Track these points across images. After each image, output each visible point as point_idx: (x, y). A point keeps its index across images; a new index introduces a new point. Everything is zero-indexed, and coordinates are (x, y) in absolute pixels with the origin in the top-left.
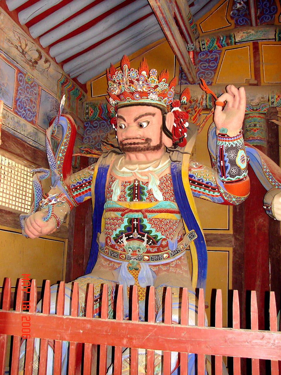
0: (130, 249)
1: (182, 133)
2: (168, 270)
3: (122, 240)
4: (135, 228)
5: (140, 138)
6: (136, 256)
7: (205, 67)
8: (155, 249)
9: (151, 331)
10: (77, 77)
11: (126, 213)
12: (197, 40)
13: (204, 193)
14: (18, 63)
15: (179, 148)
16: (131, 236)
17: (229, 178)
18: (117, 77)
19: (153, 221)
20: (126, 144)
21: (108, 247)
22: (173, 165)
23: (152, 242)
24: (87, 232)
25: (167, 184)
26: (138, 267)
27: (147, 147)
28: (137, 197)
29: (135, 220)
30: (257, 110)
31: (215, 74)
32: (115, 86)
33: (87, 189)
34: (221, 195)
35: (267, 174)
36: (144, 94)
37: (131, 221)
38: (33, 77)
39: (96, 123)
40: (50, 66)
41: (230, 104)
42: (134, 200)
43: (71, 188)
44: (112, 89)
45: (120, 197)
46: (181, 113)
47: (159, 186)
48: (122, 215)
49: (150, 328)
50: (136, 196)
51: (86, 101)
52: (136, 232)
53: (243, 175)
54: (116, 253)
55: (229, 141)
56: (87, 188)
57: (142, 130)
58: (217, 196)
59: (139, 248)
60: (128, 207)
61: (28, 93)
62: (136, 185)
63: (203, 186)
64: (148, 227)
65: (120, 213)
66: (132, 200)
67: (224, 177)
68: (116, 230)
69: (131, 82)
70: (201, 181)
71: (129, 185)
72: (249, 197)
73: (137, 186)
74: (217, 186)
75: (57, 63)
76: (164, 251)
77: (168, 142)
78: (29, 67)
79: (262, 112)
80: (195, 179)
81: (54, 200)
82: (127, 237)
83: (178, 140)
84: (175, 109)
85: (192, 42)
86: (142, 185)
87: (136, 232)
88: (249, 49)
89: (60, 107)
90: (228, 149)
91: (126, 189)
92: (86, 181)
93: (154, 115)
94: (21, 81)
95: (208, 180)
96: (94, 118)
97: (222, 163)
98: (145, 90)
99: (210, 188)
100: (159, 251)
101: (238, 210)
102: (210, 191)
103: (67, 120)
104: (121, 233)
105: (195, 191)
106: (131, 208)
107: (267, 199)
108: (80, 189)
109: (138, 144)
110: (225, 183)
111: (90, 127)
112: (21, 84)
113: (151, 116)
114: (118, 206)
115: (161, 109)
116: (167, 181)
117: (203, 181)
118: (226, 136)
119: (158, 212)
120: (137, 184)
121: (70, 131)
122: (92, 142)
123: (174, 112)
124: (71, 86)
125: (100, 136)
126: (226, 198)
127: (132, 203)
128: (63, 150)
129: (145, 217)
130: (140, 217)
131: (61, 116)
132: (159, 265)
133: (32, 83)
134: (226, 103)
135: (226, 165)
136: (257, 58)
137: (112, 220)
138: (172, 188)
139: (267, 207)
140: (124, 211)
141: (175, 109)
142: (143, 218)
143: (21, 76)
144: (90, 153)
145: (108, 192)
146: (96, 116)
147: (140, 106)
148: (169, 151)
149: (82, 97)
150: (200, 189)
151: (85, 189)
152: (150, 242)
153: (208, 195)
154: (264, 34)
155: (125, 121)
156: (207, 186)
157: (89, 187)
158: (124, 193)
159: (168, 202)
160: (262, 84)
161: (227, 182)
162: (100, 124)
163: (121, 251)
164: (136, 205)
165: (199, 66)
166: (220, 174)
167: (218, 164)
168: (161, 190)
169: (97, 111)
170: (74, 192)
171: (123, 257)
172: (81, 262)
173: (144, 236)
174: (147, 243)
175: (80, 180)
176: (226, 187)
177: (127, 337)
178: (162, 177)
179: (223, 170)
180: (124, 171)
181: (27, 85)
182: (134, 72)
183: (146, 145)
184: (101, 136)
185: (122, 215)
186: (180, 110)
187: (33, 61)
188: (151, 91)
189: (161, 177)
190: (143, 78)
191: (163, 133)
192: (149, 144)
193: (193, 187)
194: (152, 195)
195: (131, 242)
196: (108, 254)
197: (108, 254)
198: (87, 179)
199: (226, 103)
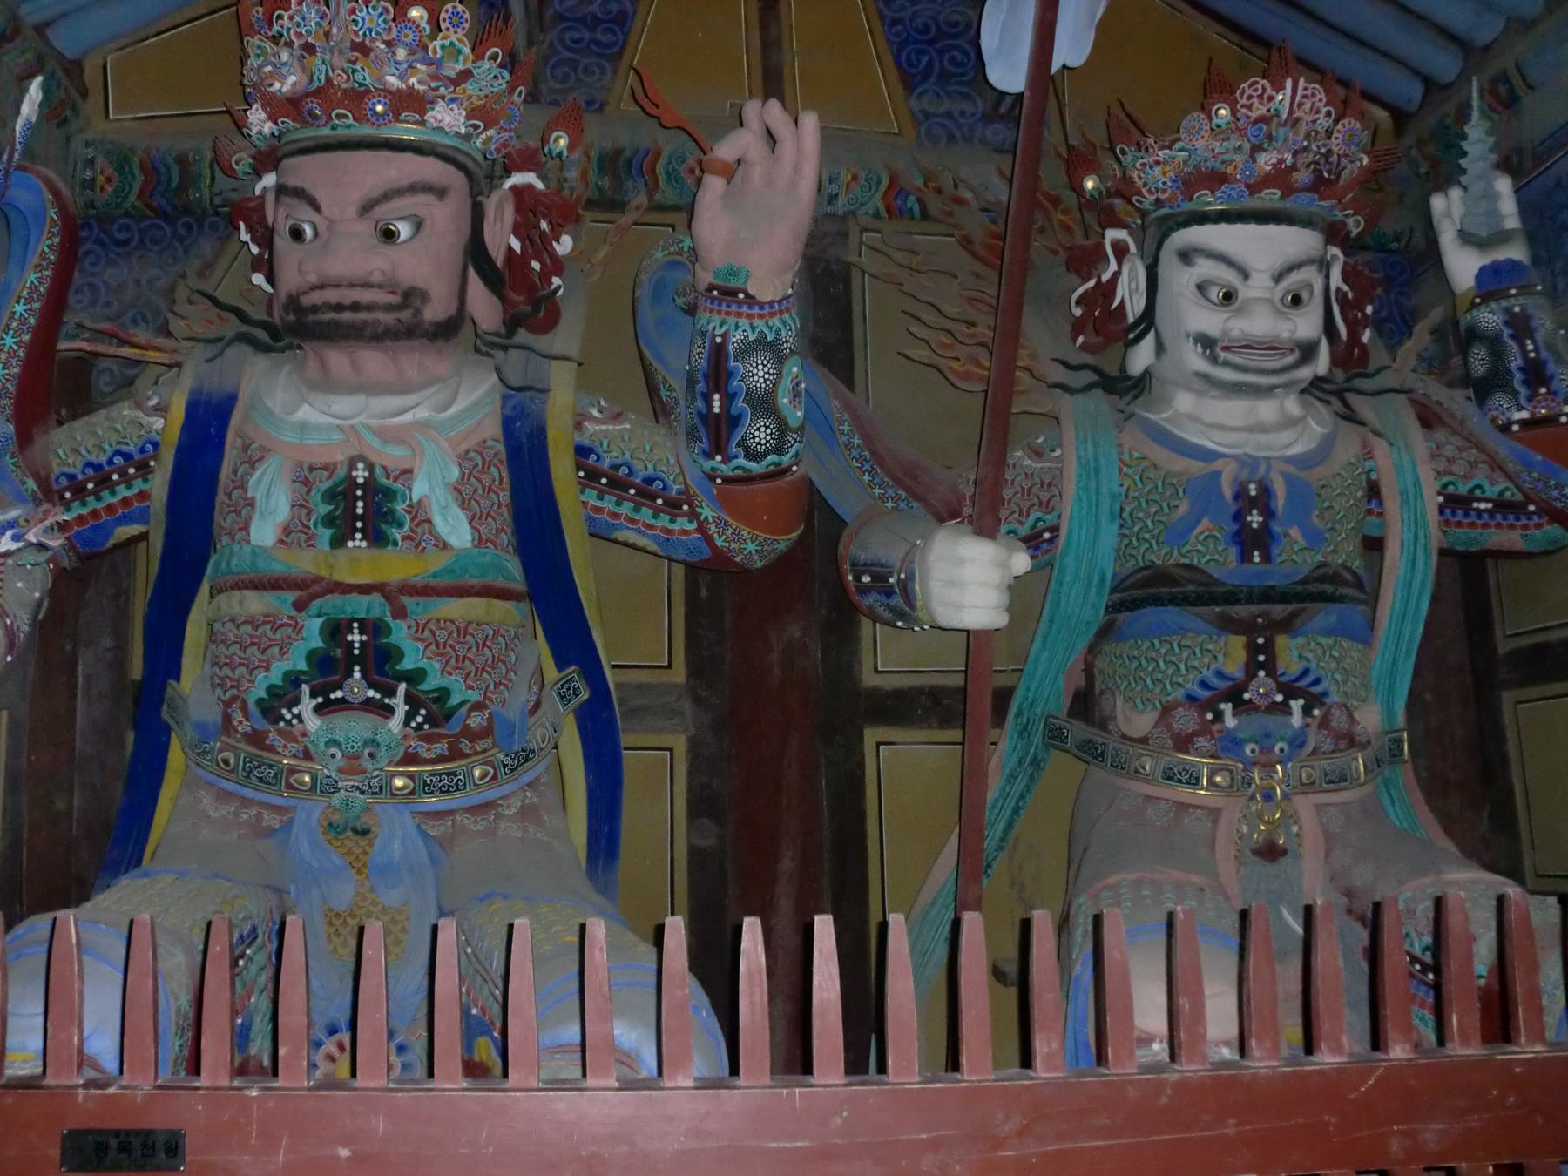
0: (333, 750)
1: (545, 276)
2: (491, 832)
3: (295, 711)
4: (356, 661)
5: (380, 286)
6: (360, 777)
7: (577, 41)
8: (441, 748)
13: (633, 521)
15: (523, 336)
16: (339, 694)
17: (742, 461)
18: (297, 19)
19: (433, 633)
20: (315, 309)
21: (231, 741)
22: (510, 404)
23: (427, 719)
24: (88, 678)
25: (486, 479)
26: (365, 821)
28: (361, 531)
29: (355, 625)
31: (615, 72)
32: (285, 56)
33: (128, 493)
34: (702, 529)
35: (854, 453)
36: (409, 103)
37: (335, 630)
39: (127, 228)
42: (350, 544)
43: (56, 487)
44: (269, 68)
45: (287, 530)
47: (456, 489)
48: (300, 606)
50: (359, 524)
51: (81, 130)
52: (357, 675)
53: (792, 451)
54: (271, 767)
55: (750, 317)
56: (129, 487)
57: (390, 250)
58: (686, 532)
59: (373, 742)
60: (324, 573)
63: (632, 491)
65: (291, 596)
66: (338, 542)
67: (719, 458)
68: (267, 669)
69: (363, 49)
70: (623, 471)
71: (330, 477)
72: (801, 537)
73: (363, 486)
74: (686, 491)
76: (477, 753)
77: (484, 307)
80: (598, 465)
81: (9, 533)
82: (320, 700)
83: (526, 299)
84: (518, 179)
86: (384, 481)
87: (357, 675)
91: (316, 497)
92: (127, 457)
93: (441, 192)
95: (650, 467)
96: (118, 206)
97: (716, 404)
99: (660, 501)
100: (455, 754)
101: (704, 593)
103: (45, 190)
104: (294, 680)
105: (598, 510)
106: (337, 577)
108: (96, 494)
109: (370, 308)
110: (719, 481)
111: (99, 242)
113: (429, 198)
114: (278, 568)
116: (486, 466)
117: (631, 473)
118: (741, 296)
119: (451, 595)
120: (360, 474)
121: (57, 240)
122: (108, 304)
124: (29, 56)
125: (144, 282)
126: (719, 543)
127: (340, 553)
129: (400, 613)
130: (376, 613)
131: (19, 168)
132: (451, 812)
135: (734, 412)
137: (248, 628)
138: (505, 496)
140: (307, 590)
141: (518, 179)
142: (389, 619)
144: (123, 342)
145: (226, 509)
146: (126, 197)
147: (385, 154)
148: (484, 349)
149: (68, 113)
150: (618, 504)
151: (122, 492)
152: (419, 719)
153: (651, 527)
155: (317, 208)
156: (646, 493)
157: (138, 485)
158: (304, 511)
159: (490, 554)
161: (726, 480)
162: (140, 230)
163: (294, 756)
164: (358, 560)
165: (552, 36)
166: (705, 444)
167: (700, 404)
168: (464, 504)
169: (134, 177)
172: (60, 805)
173: (392, 693)
174: (407, 724)
175: (95, 452)
176: (725, 502)
178: (467, 452)
179: (718, 429)
182: (374, 8)
183: (405, 315)
184: (149, 282)
185: (300, 606)
186: (540, 185)
189: (464, 447)
190: (410, 37)
191: (472, 272)
192: (418, 312)
193: (591, 497)
194: (426, 526)
196: (232, 771)
197: (232, 771)
198: (131, 448)
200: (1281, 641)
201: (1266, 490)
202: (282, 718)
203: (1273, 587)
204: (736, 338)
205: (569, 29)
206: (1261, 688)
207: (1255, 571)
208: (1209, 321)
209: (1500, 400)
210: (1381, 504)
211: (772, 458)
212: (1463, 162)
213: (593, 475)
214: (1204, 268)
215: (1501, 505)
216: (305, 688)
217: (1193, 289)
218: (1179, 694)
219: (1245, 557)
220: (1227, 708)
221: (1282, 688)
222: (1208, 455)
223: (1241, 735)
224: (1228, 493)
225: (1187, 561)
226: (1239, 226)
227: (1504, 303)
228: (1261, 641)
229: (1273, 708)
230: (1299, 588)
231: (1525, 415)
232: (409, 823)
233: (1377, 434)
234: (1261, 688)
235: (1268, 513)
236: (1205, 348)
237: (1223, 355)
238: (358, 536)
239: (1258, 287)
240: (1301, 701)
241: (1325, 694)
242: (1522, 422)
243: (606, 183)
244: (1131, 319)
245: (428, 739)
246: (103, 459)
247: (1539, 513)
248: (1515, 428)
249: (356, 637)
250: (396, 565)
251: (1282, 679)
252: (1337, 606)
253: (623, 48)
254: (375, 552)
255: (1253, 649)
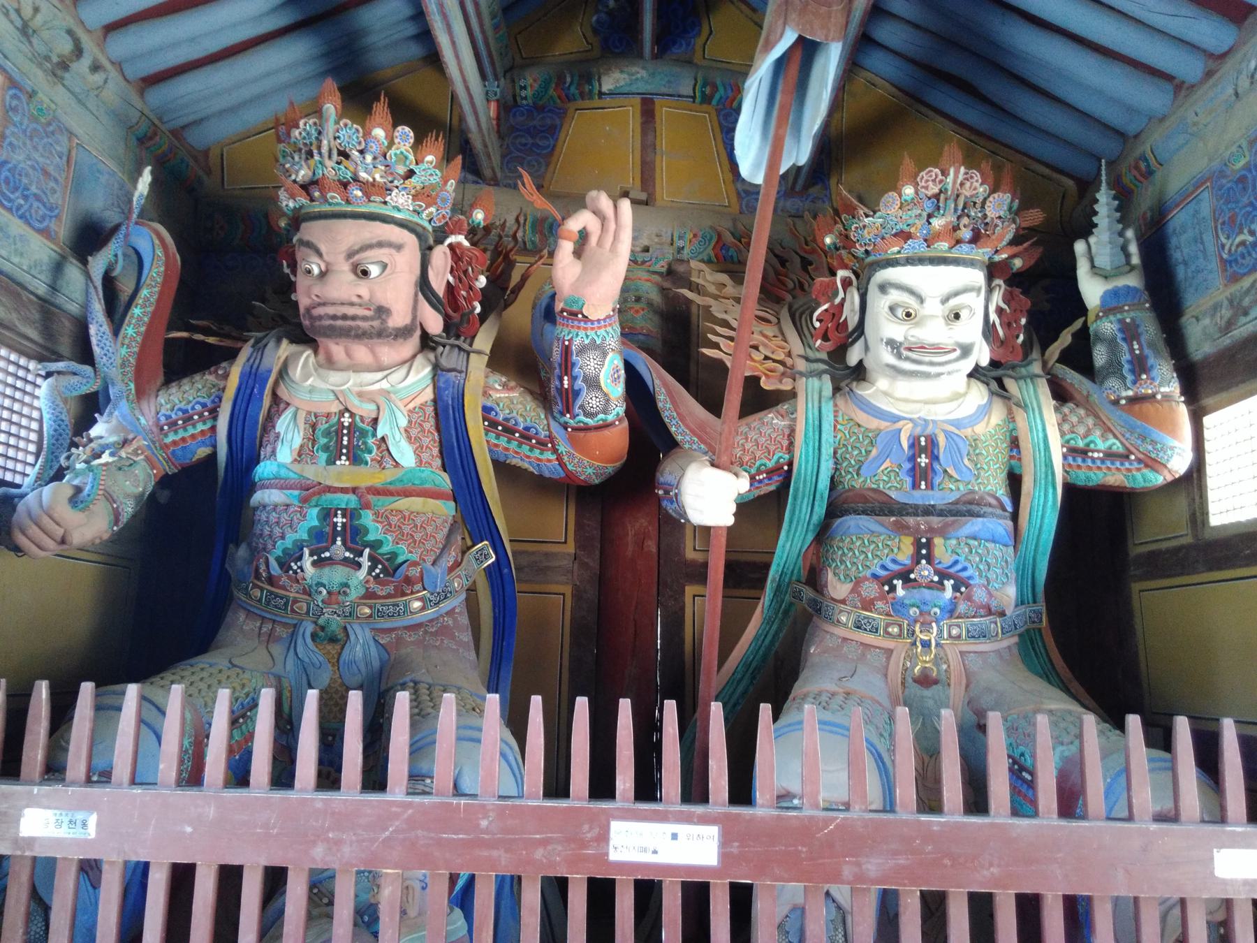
1: (469, 300)
7: (525, 145)
9: (397, 816)
10: (183, 128)
11: (314, 494)
12: (508, 75)
13: (517, 453)
14: (5, 57)
16: (327, 554)
17: (582, 418)
20: (320, 318)
27: (373, 328)
30: (644, 262)
34: (559, 459)
36: (370, 189)
37: (327, 514)
38: (53, 106)
40: (106, 82)
41: (593, 240)
42: (338, 463)
46: (468, 250)
48: (305, 500)
49: (394, 809)
52: (339, 543)
55: (585, 329)
58: (549, 461)
61: (35, 148)
62: (346, 424)
64: (375, 531)
66: (331, 462)
69: (344, 154)
73: (349, 428)
75: (126, 79)
78: (40, 73)
79: (657, 268)
81: (107, 452)
85: (496, 78)
86: (361, 424)
87: (339, 543)
88: (631, 113)
89: (135, 199)
90: (583, 350)
93: (399, 247)
94: (15, 110)
98: (377, 177)
102: (532, 448)
103: (154, 237)
105: (496, 445)
106: (329, 483)
107: (666, 474)
109: (354, 318)
112: (16, 119)
113: (393, 251)
115: (419, 236)
117: (516, 424)
120: (346, 420)
123: (451, 246)
126: (570, 467)
128: (140, 319)
131: (137, 223)
133: (49, 124)
134: (584, 235)
135: (576, 388)
136: (650, 137)
139: (667, 492)
141: (452, 239)
143: (15, 97)
147: (363, 221)
151: (181, 434)
152: (377, 571)
153: (528, 457)
154: (669, 82)
156: (526, 437)
159: (426, 473)
160: (659, 202)
164: (342, 472)
170: (166, 435)
171: (300, 608)
173: (361, 555)
174: (369, 573)
176: (573, 442)
177: (327, 840)
180: (315, 385)
181: (35, 125)
183: (376, 323)
187: (55, 59)
188: (396, 183)
189: (411, 406)
191: (420, 296)
192: (384, 322)
195: (326, 570)
199: (584, 235)
200: (938, 541)
201: (932, 441)
202: (291, 568)
203: (933, 506)
204: (577, 341)
205: (516, 137)
206: (925, 571)
207: (923, 496)
208: (897, 331)
209: (1113, 383)
210: (1019, 452)
211: (601, 416)
212: (1095, 219)
213: (493, 424)
214: (895, 296)
215: (1110, 455)
216: (306, 551)
217: (887, 309)
218: (868, 573)
219: (915, 486)
220: (898, 583)
221: (937, 572)
222: (896, 419)
223: (907, 602)
224: (905, 445)
225: (874, 486)
226: (920, 268)
227: (1119, 316)
228: (924, 540)
229: (930, 586)
230: (953, 507)
231: (1130, 393)
232: (368, 634)
233: (1018, 405)
234: (925, 571)
235: (934, 458)
236: (893, 348)
237: (905, 353)
238: (344, 458)
239: (933, 307)
240: (952, 582)
241: (970, 578)
242: (1127, 398)
243: (537, 239)
244: (850, 329)
245: (383, 583)
246: (189, 407)
247: (1139, 461)
248: (1123, 402)
249: (339, 520)
250: (367, 476)
251: (939, 566)
252: (980, 519)
253: (553, 149)
254: (353, 468)
255: (918, 545)
